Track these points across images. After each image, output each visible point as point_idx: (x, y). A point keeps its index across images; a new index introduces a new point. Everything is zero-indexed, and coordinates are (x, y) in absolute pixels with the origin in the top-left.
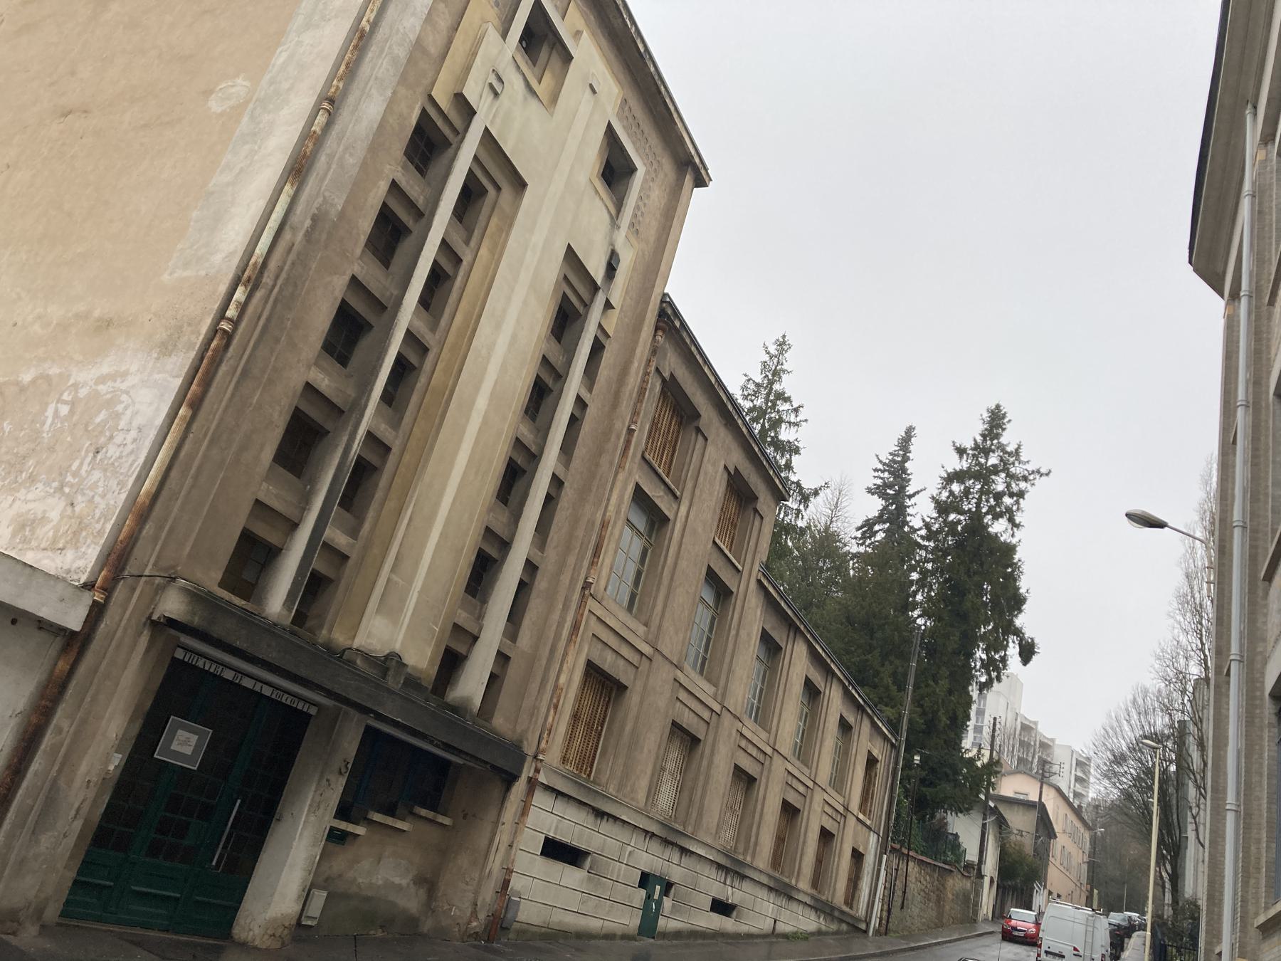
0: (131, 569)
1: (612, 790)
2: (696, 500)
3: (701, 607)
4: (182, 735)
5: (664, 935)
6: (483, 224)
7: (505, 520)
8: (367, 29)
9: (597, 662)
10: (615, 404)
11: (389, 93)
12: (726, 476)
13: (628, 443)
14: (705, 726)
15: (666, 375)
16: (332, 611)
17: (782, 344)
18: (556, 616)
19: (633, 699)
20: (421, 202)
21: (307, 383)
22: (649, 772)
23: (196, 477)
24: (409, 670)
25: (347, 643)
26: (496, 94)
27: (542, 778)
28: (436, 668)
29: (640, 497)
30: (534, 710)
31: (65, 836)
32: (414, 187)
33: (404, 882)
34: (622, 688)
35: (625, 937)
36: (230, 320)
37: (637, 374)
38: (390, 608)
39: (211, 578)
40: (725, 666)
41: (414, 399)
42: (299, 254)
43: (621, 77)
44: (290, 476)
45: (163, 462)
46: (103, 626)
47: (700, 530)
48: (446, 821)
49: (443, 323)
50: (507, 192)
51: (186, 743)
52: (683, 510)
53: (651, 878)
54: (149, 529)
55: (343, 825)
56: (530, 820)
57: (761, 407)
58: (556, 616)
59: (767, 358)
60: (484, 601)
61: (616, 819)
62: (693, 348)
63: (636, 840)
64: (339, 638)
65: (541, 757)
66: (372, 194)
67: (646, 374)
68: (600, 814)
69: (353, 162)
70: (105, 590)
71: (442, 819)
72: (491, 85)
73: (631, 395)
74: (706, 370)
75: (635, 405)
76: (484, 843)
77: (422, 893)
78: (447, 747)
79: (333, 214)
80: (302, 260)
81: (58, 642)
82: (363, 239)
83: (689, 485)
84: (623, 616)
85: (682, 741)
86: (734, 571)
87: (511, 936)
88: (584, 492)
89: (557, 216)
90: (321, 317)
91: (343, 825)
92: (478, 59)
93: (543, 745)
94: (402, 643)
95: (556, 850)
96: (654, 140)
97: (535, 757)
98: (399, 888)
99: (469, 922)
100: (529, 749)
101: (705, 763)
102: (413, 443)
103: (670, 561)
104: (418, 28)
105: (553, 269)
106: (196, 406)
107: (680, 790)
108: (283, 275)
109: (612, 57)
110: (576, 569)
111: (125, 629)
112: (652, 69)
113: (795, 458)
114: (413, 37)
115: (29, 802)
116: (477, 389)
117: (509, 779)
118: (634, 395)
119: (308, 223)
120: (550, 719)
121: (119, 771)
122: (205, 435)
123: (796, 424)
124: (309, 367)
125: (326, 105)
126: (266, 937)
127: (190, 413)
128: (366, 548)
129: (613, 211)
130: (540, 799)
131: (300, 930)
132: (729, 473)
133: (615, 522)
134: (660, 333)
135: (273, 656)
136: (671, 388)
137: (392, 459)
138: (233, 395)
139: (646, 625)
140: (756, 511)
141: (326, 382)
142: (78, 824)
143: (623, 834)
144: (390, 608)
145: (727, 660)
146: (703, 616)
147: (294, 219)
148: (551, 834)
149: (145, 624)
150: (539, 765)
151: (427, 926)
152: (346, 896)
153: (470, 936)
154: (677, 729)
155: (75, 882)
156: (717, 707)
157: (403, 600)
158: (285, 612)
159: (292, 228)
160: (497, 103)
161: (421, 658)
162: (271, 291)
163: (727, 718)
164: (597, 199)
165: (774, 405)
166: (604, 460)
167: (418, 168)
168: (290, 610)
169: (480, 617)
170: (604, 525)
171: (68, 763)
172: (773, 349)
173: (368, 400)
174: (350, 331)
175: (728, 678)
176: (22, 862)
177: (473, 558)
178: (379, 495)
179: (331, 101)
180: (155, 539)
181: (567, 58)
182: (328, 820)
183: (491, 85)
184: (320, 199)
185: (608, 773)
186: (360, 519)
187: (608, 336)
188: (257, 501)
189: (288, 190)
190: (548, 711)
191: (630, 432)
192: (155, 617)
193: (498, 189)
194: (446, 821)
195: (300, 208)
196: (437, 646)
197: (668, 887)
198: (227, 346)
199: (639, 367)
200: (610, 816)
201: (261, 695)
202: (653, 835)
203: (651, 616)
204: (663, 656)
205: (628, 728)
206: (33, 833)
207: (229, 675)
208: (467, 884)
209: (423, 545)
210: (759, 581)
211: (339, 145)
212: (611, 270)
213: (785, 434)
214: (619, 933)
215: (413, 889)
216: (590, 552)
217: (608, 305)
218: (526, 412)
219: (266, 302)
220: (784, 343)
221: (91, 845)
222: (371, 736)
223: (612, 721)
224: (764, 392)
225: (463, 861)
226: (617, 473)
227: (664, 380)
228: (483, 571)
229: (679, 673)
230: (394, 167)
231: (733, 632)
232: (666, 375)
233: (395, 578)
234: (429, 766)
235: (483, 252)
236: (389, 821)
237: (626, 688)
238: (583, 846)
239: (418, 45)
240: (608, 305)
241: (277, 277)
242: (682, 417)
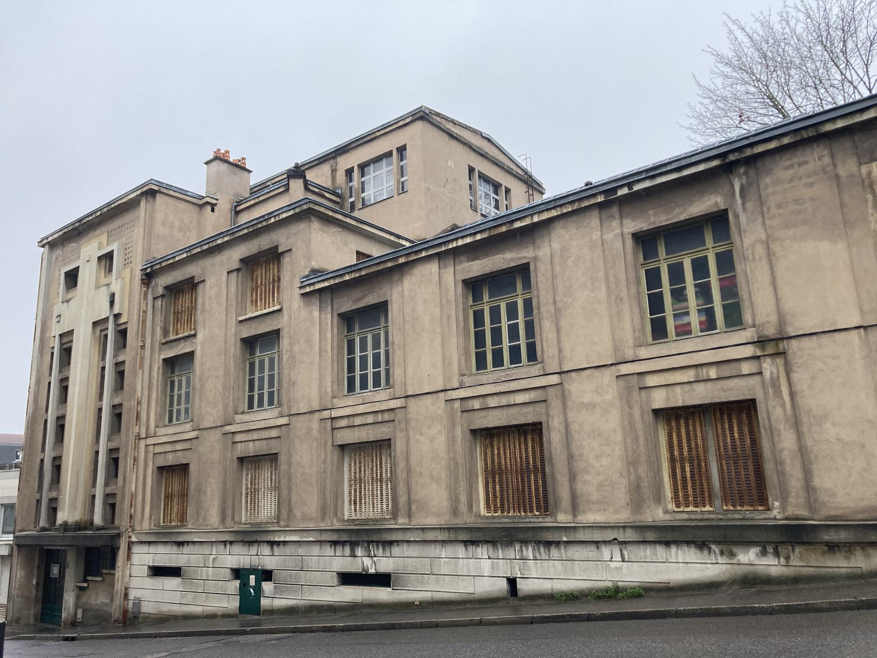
5: (272, 612)
27: (134, 539)
56: (135, 559)
61: (194, 543)
68: (180, 544)
95: (158, 571)
109: (86, 239)
130: (136, 549)
143: (206, 549)
148: (151, 564)
202: (231, 543)
214: (220, 613)
238: (174, 565)
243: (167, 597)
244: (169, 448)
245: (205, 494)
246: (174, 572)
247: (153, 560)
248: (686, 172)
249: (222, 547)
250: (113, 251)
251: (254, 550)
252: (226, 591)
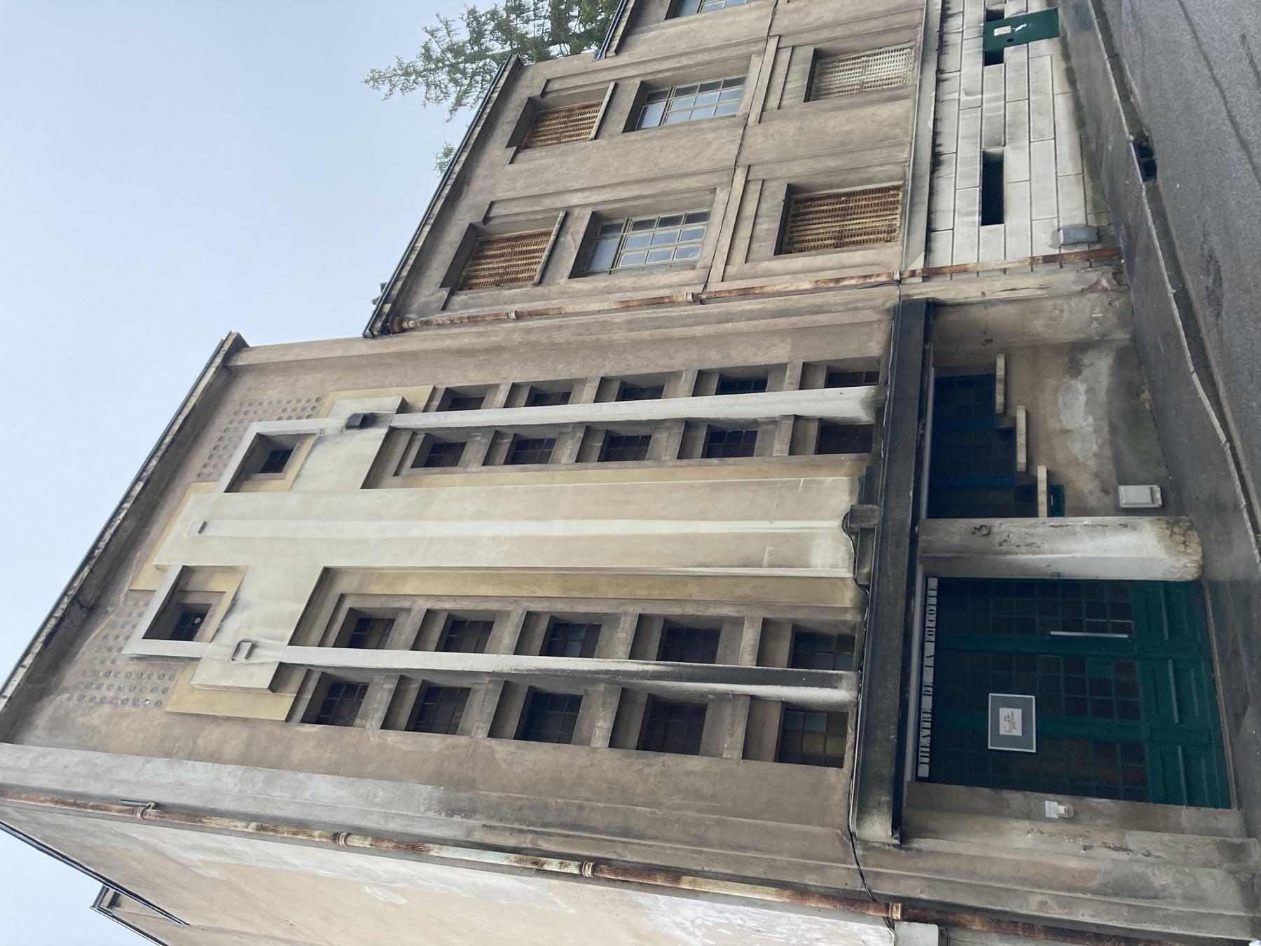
0: (857, 885)
1: (905, 154)
2: (560, 187)
3: (672, 119)
4: (1004, 729)
6: (384, 600)
7: (665, 435)
8: (254, 825)
9: (772, 243)
10: (495, 350)
11: (301, 776)
12: (520, 156)
13: (532, 314)
14: (797, 51)
15: (444, 293)
16: (824, 617)
17: (376, 79)
18: (742, 326)
19: (798, 171)
20: (390, 686)
21: (610, 746)
22: (869, 111)
23: (740, 848)
24: (854, 502)
25: (851, 584)
26: (254, 646)
27: (918, 264)
28: (843, 457)
29: (582, 269)
30: (852, 308)
31: (1148, 855)
32: (378, 701)
33: (1082, 387)
34: (791, 190)
35: (1066, 56)
36: (580, 867)
37: (457, 336)
38: (800, 545)
39: (838, 780)
40: (725, 54)
41: (581, 608)
42: (490, 817)
43: (178, 491)
44: (708, 716)
45: (744, 890)
46: (924, 896)
47: (589, 165)
48: (1001, 363)
49: (494, 606)
50: (343, 585)
51: (1010, 719)
52: (576, 199)
53: (990, 49)
54: (811, 880)
55: (1042, 498)
56: (965, 257)
57: (449, 72)
58: (742, 326)
59: (397, 91)
60: (755, 422)
61: (935, 134)
62: (405, 273)
63: (951, 91)
64: (848, 597)
65: (897, 277)
66: (404, 748)
67: (452, 323)
68: (936, 160)
69: (381, 791)
70: (887, 905)
71: (1000, 373)
72: (248, 656)
73: (482, 334)
74: (419, 244)
75: (490, 322)
76: (1011, 310)
77: (1087, 359)
78: (922, 414)
79: (438, 793)
80: (494, 810)
81: (956, 934)
82: (450, 739)
83: (548, 203)
84: (716, 218)
85: (823, 74)
86: (619, 91)
87: (1104, 223)
88: (603, 348)
89: (339, 521)
90: (539, 757)
91: (1042, 498)
92: (229, 683)
93: (883, 279)
94: (830, 519)
95: (992, 211)
96: (222, 421)
97: (899, 282)
98: (1090, 391)
99: (1105, 290)
100: (891, 296)
101: (839, 32)
102: (624, 593)
103: (635, 191)
104: (230, 768)
105: (393, 496)
106: (675, 874)
107: (878, 50)
108: (516, 826)
109: (170, 503)
110: (684, 322)
111: (919, 870)
112: (154, 462)
113: (481, 10)
114: (239, 770)
115: (1125, 911)
116: (543, 540)
117: (934, 307)
118: (481, 329)
119: (457, 818)
120: (853, 282)
121: (1060, 797)
122: (700, 852)
123: (447, 25)
124: (594, 750)
125: (342, 842)
126: (1189, 551)
127: (685, 878)
128: (746, 602)
129: (310, 442)
130: (942, 258)
131: (1171, 509)
132: (517, 152)
133: (620, 290)
134: (405, 325)
135: (893, 684)
136: (457, 281)
137: (650, 610)
138: (651, 838)
139: (714, 191)
140: (544, 93)
141: (600, 723)
142: (1136, 839)
143: (949, 111)
144: (802, 543)
145: (716, 55)
146: (682, 109)
147: (459, 835)
148: (977, 218)
149: (906, 849)
150: (906, 274)
151: (1122, 336)
152: (1117, 459)
153: (1119, 283)
154: (813, 92)
155: (1191, 804)
156: (772, 44)
157: (787, 538)
158: (844, 683)
159: (469, 834)
160: (262, 641)
161: (835, 486)
162: (536, 832)
163: (782, 24)
164: (304, 472)
165: (438, 61)
166: (560, 338)
167: (362, 695)
168: (840, 677)
169: (773, 422)
170: (627, 306)
171: (1073, 886)
172: (386, 88)
173: (601, 672)
174: (542, 714)
175: (735, 45)
176: (1188, 899)
177: (715, 461)
178: (691, 610)
179: (335, 837)
180: (818, 869)
181: (186, 571)
182: (1041, 525)
183: (248, 656)
184: (431, 814)
185: (886, 168)
186: (722, 620)
187: (435, 389)
188: (745, 756)
189: (435, 851)
190: (845, 287)
191: (519, 316)
192: (897, 842)
193: (342, 597)
194: (1001, 363)
195: (447, 833)
196: (818, 467)
197: (993, 18)
198: (607, 861)
199: (450, 336)
200: (935, 145)
201: (936, 656)
202: (939, 71)
203: (700, 189)
204: (739, 153)
205: (832, 163)
206: (1156, 897)
207: (927, 703)
208: (1062, 311)
209: (722, 537)
210: (617, 52)
211: (372, 813)
212: (367, 421)
213: (463, 35)
214: (1063, 65)
215: (1086, 372)
216: (661, 312)
217: (404, 408)
218: (546, 462)
219: (550, 834)
220: (372, 78)
221: (1146, 800)
222: (939, 509)
223: (832, 186)
224: (431, 78)
225: (1038, 326)
226: (568, 315)
227: (452, 293)
228: (727, 441)
229: (753, 118)
230: (367, 733)
231: (685, 61)
232: (444, 293)
233: (766, 558)
234: (944, 416)
235: (408, 590)
236: (1021, 440)
237: (789, 186)
238: (978, 167)
239: (244, 760)
240: (404, 408)
241: (521, 831)
242: (482, 243)
243: (1044, 165)
244: (745, 232)
245: (848, 133)
246: (992, 170)
247: (968, 214)
248: (472, 141)
249: (946, 86)
250: (149, 635)
251: (953, 38)
252: (1022, 64)
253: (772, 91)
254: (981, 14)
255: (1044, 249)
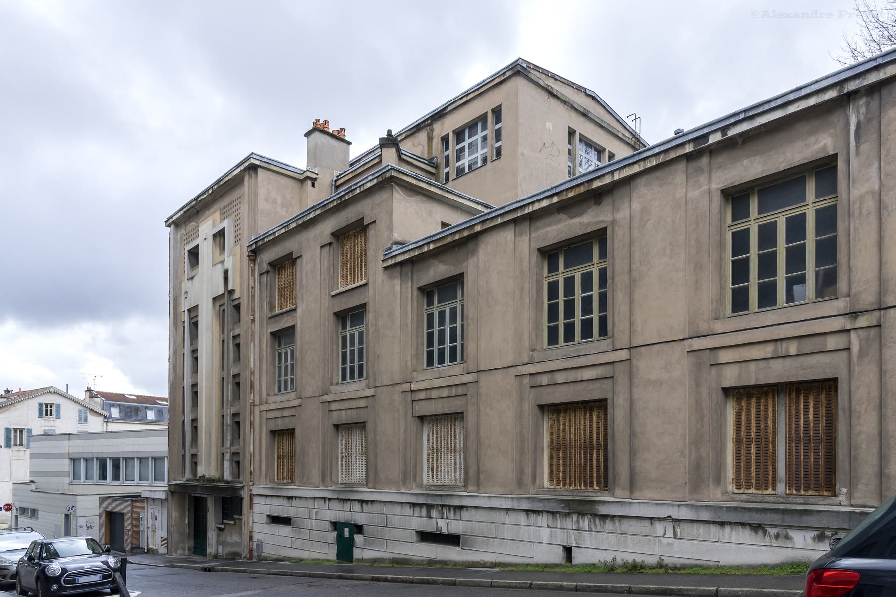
6: (846, 388)
27: (254, 492)
56: (257, 508)
95: (275, 520)
130: (256, 500)
143: (309, 504)
197: (359, 529)
238: (285, 516)
246: (285, 521)
251: (347, 506)
253: (342, 403)
254: (359, 523)
255: (256, 537)
